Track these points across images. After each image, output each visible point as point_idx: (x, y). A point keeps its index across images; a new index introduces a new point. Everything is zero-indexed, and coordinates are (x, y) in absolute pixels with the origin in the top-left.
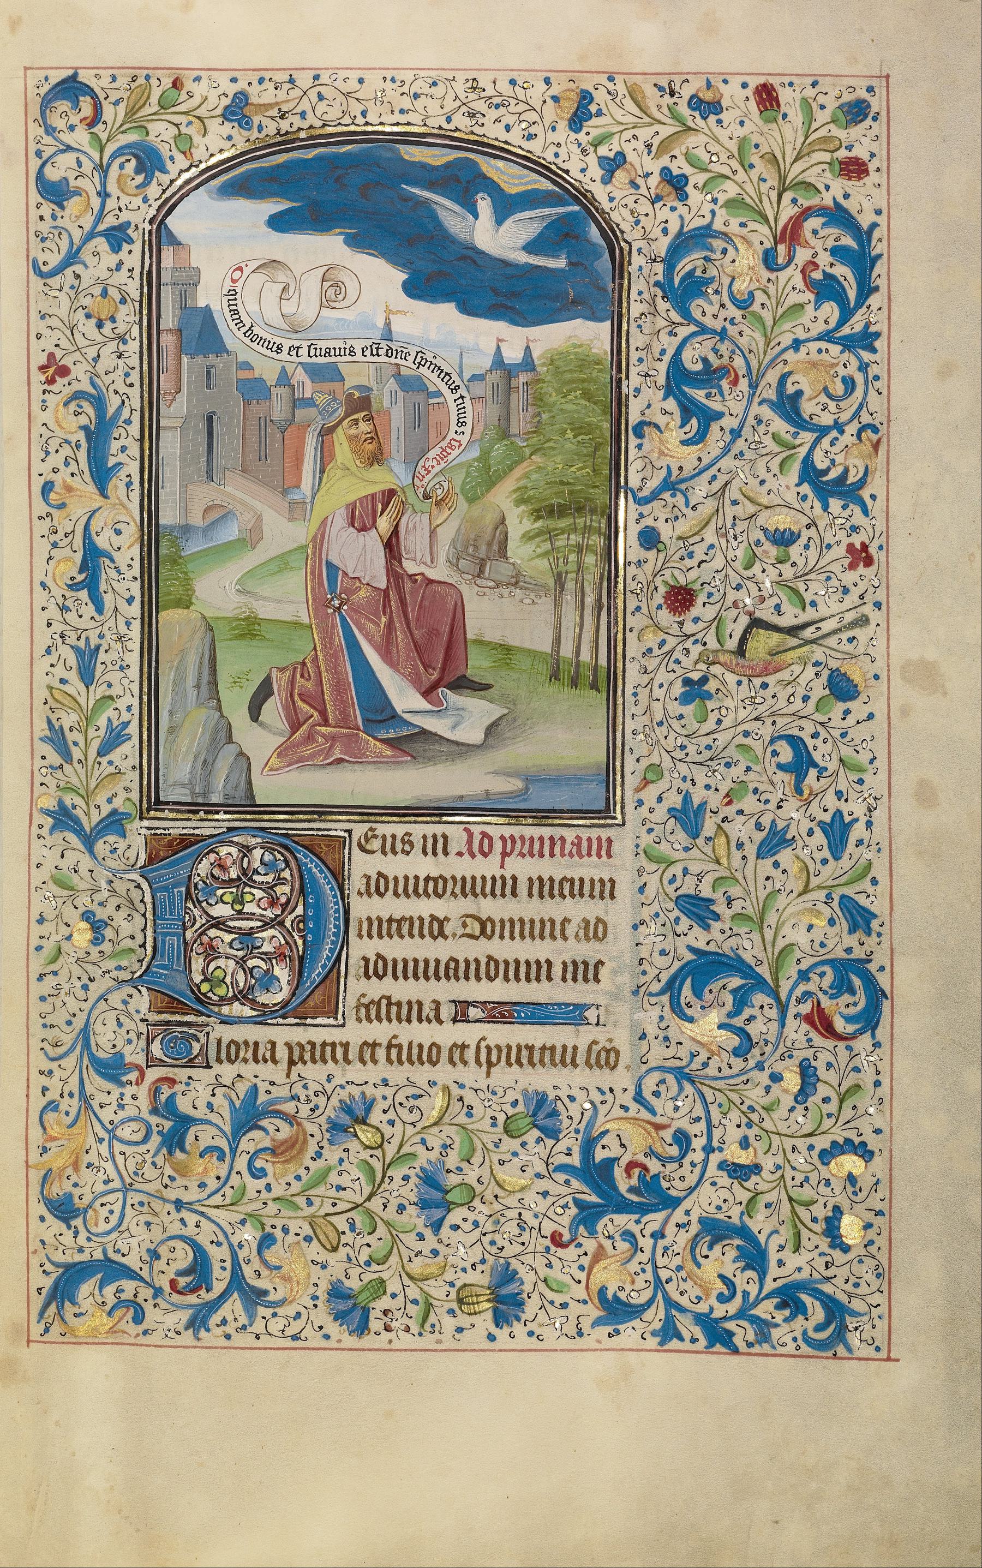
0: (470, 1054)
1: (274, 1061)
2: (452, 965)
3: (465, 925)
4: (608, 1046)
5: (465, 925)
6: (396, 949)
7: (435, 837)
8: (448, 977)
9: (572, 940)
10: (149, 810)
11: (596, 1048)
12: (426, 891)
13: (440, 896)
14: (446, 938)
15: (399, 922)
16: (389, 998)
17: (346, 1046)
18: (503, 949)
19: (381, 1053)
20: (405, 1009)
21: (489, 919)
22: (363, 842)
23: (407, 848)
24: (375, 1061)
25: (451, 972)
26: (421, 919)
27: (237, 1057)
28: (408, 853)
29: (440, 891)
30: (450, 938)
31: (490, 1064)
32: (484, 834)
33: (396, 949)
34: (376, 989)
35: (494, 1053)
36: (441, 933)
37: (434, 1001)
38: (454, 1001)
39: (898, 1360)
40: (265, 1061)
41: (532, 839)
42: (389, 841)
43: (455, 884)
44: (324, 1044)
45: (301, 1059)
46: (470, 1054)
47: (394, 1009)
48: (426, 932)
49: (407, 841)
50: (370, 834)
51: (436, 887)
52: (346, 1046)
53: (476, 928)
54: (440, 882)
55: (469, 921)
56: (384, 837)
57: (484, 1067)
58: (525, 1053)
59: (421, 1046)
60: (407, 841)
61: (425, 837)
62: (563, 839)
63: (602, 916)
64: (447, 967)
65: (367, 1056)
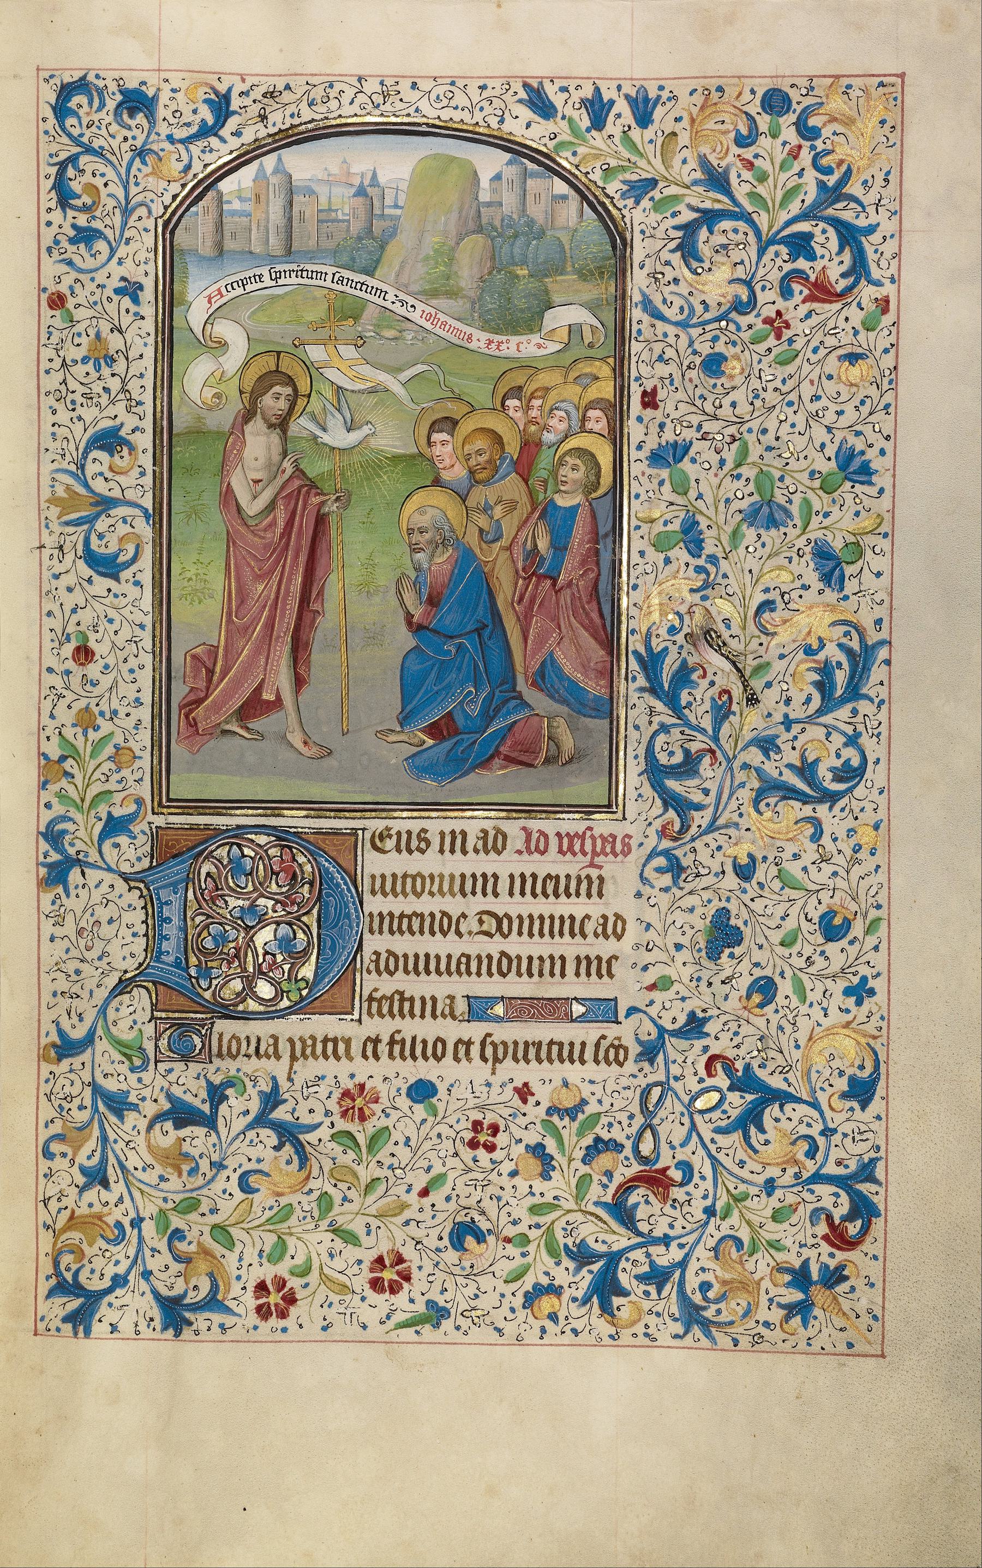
0: (475, 1050)
1: (278, 1057)
3: (481, 922)
4: (616, 1042)
6: (404, 945)
8: (459, 972)
9: (591, 938)
12: (393, 889)
14: (459, 933)
15: (409, 917)
16: (401, 994)
17: (348, 1042)
18: (517, 946)
19: (383, 1048)
20: (418, 1005)
21: (506, 915)
23: (423, 845)
24: (376, 1057)
25: (463, 967)
26: (432, 915)
28: (423, 852)
29: (419, 889)
30: (466, 937)
31: (496, 1060)
32: (541, 833)
33: (404, 945)
34: (387, 985)
37: (273, 1036)
38: (468, 997)
42: (404, 837)
43: (432, 883)
46: (475, 1050)
47: (407, 1005)
48: (436, 928)
49: (422, 836)
50: (385, 833)
53: (490, 924)
54: (419, 881)
55: (485, 917)
59: (424, 1042)
60: (422, 836)
61: (442, 834)
64: (459, 963)
65: (369, 1052)
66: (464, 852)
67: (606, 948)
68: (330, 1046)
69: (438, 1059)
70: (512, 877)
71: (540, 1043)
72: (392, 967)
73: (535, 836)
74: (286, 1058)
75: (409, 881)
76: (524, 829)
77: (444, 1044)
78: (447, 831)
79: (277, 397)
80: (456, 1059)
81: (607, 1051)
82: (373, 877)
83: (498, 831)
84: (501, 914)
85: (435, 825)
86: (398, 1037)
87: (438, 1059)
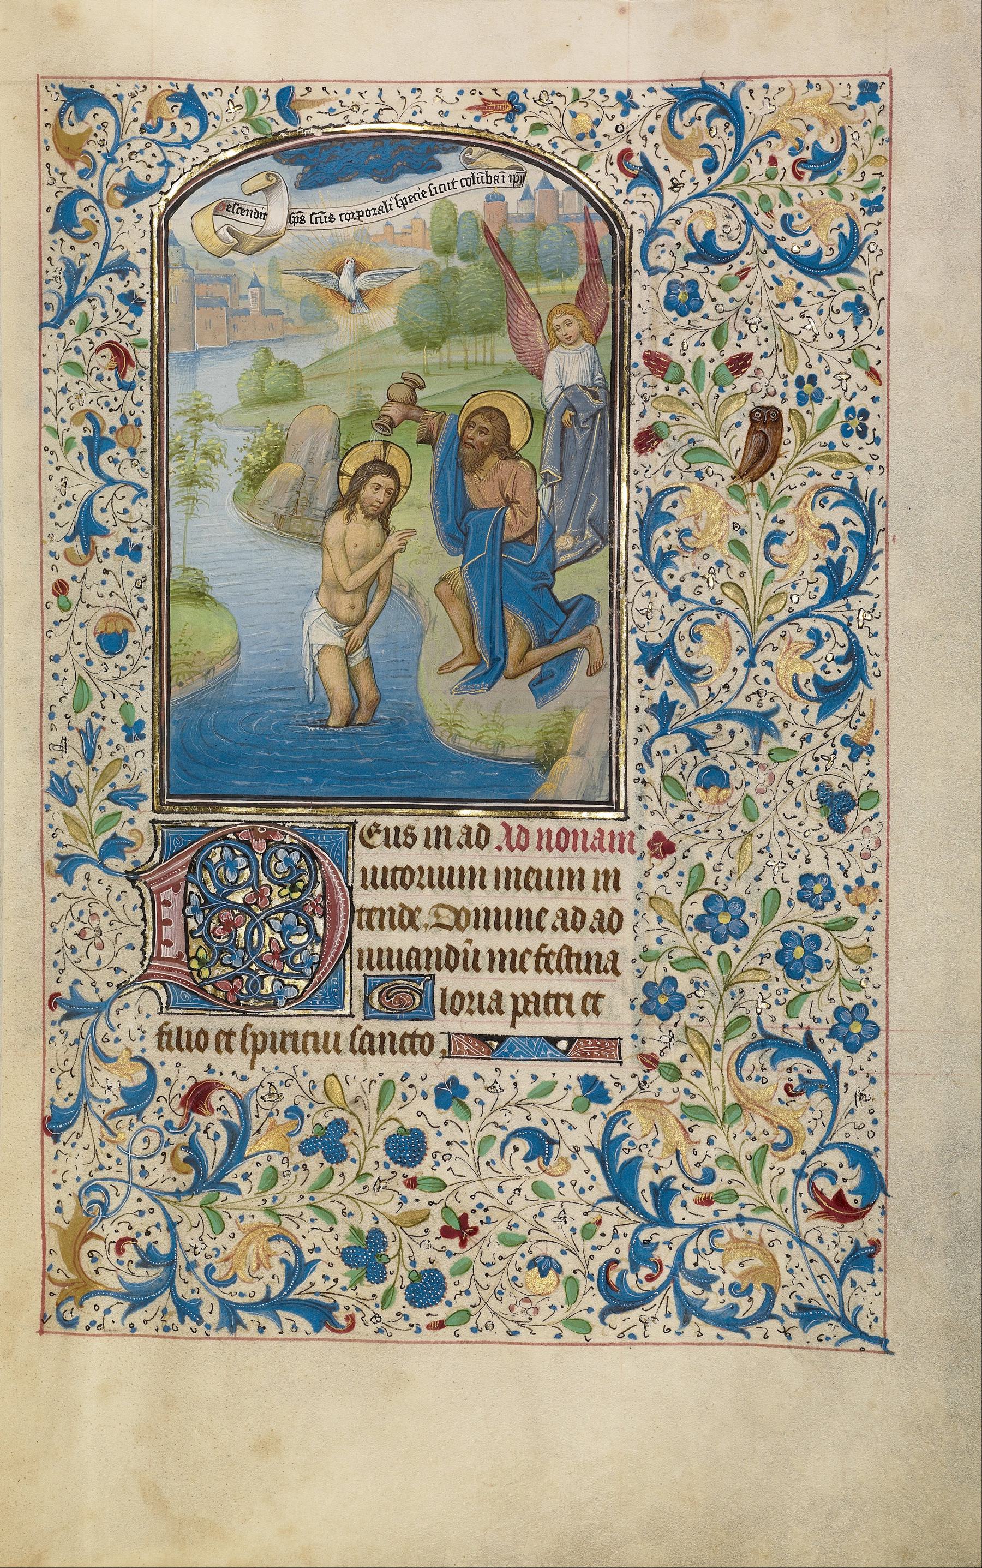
0: (236, 1041)
1: (501, 1013)
2: (414, 954)
3: (437, 915)
5: (437, 915)
7: (438, 829)
10: (618, 810)
11: (359, 1034)
13: (407, 887)
14: (417, 929)
15: (370, 912)
17: (569, 998)
22: (365, 833)
23: (409, 840)
24: (229, 1049)
25: (413, 962)
26: (392, 910)
27: (461, 1008)
28: (410, 846)
31: (256, 1051)
35: (260, 1039)
36: (412, 923)
39: (892, 1353)
40: (491, 1011)
41: (612, 833)
44: (306, 1034)
45: (526, 1010)
51: (403, 878)
52: (569, 998)
55: (442, 911)
56: (387, 829)
57: (250, 1055)
58: (289, 1041)
59: (189, 1033)
61: (428, 830)
62: (585, 833)
63: (579, 905)
65: (589, 1006)
66: (448, 846)
67: (602, 943)
68: (552, 1002)
69: (202, 1050)
70: (497, 871)
71: (296, 1033)
72: (452, 963)
73: (515, 832)
74: (508, 1016)
75: (399, 874)
76: (504, 824)
77: (206, 1035)
78: (433, 828)
79: (378, 487)
80: (218, 1049)
81: (362, 1039)
82: (364, 870)
83: (481, 826)
84: (459, 908)
85: (423, 823)
86: (166, 1029)
87: (202, 1050)
